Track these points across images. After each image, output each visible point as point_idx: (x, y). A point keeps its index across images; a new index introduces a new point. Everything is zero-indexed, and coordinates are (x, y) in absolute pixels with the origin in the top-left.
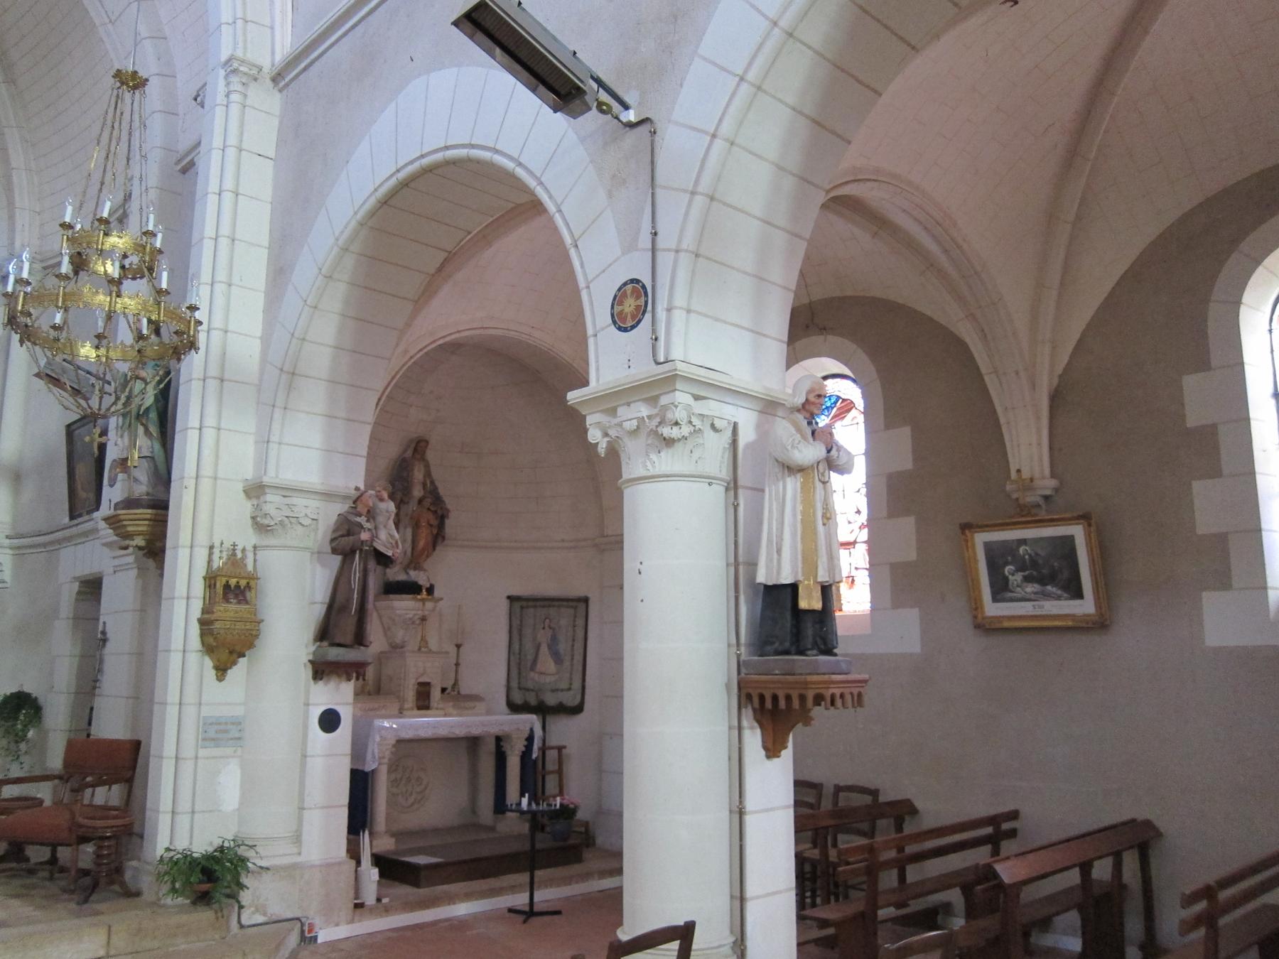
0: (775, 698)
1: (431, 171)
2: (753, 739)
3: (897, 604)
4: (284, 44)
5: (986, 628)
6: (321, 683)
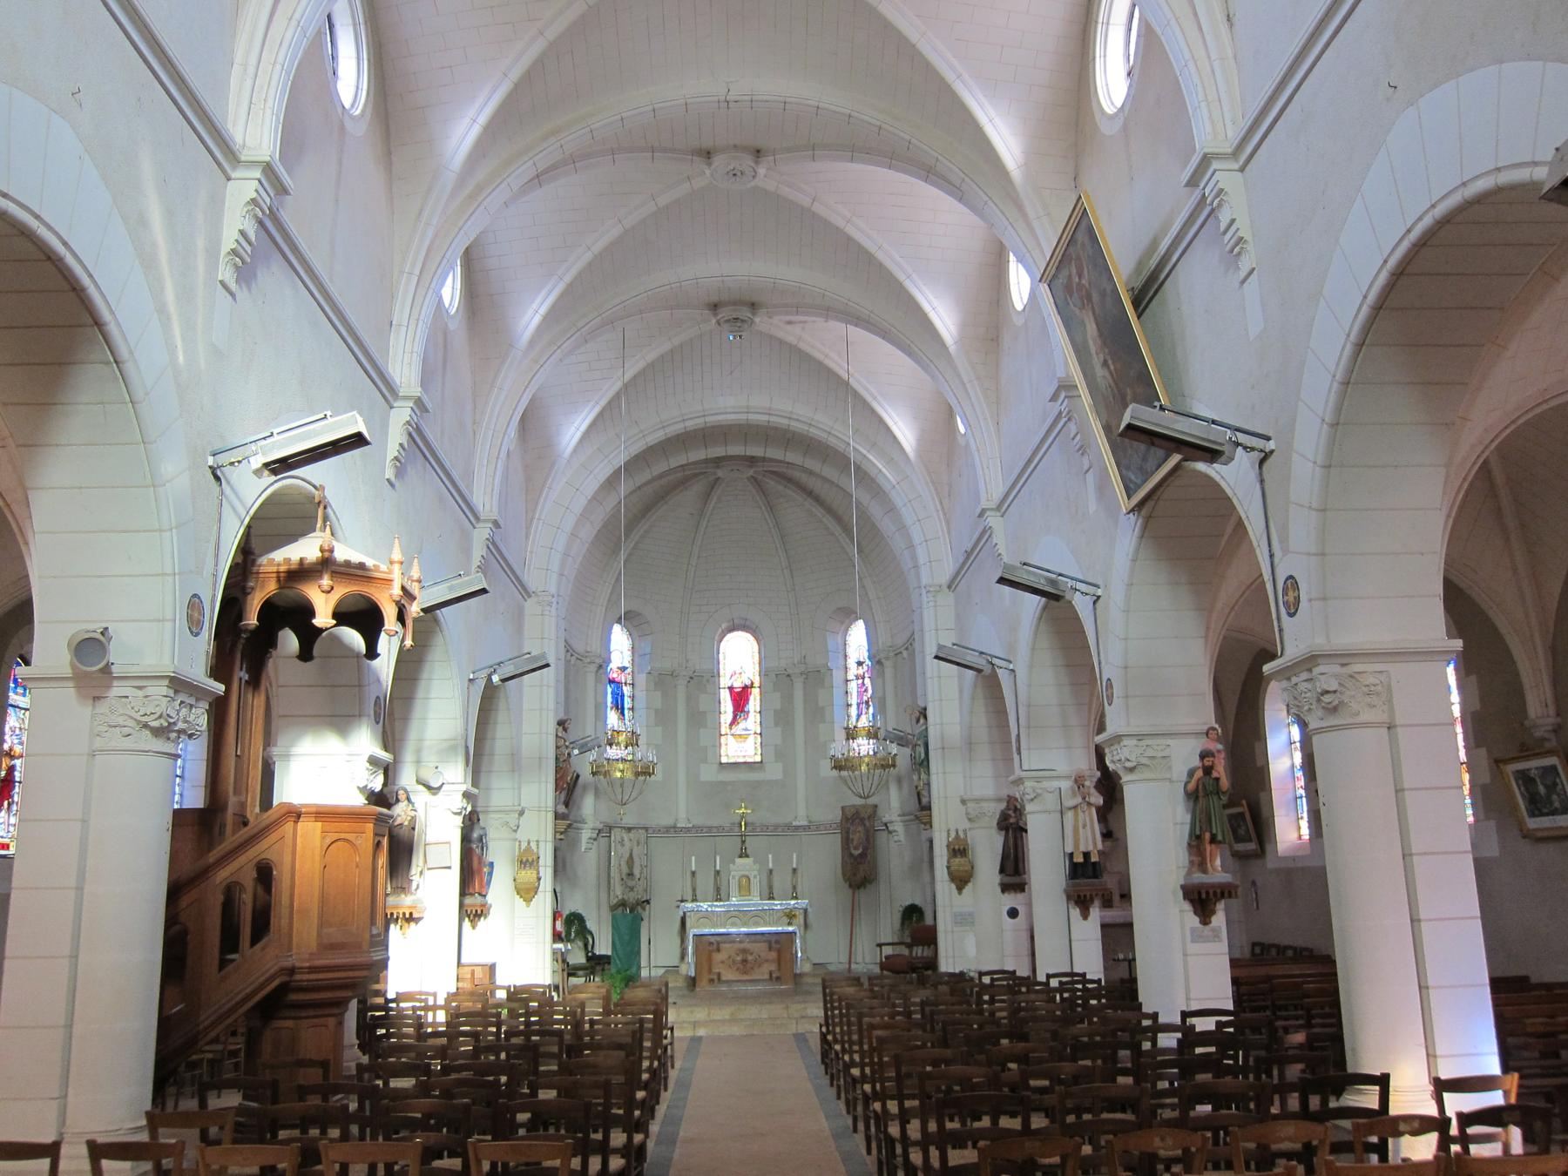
0: (1207, 893)
1: (1424, 244)
2: (1075, 912)
3: (1487, 818)
4: (1233, 134)
5: (1527, 835)
6: (1006, 894)
